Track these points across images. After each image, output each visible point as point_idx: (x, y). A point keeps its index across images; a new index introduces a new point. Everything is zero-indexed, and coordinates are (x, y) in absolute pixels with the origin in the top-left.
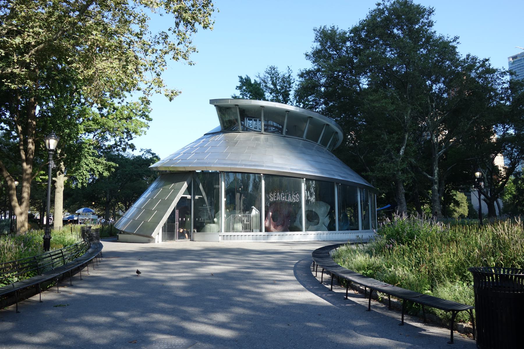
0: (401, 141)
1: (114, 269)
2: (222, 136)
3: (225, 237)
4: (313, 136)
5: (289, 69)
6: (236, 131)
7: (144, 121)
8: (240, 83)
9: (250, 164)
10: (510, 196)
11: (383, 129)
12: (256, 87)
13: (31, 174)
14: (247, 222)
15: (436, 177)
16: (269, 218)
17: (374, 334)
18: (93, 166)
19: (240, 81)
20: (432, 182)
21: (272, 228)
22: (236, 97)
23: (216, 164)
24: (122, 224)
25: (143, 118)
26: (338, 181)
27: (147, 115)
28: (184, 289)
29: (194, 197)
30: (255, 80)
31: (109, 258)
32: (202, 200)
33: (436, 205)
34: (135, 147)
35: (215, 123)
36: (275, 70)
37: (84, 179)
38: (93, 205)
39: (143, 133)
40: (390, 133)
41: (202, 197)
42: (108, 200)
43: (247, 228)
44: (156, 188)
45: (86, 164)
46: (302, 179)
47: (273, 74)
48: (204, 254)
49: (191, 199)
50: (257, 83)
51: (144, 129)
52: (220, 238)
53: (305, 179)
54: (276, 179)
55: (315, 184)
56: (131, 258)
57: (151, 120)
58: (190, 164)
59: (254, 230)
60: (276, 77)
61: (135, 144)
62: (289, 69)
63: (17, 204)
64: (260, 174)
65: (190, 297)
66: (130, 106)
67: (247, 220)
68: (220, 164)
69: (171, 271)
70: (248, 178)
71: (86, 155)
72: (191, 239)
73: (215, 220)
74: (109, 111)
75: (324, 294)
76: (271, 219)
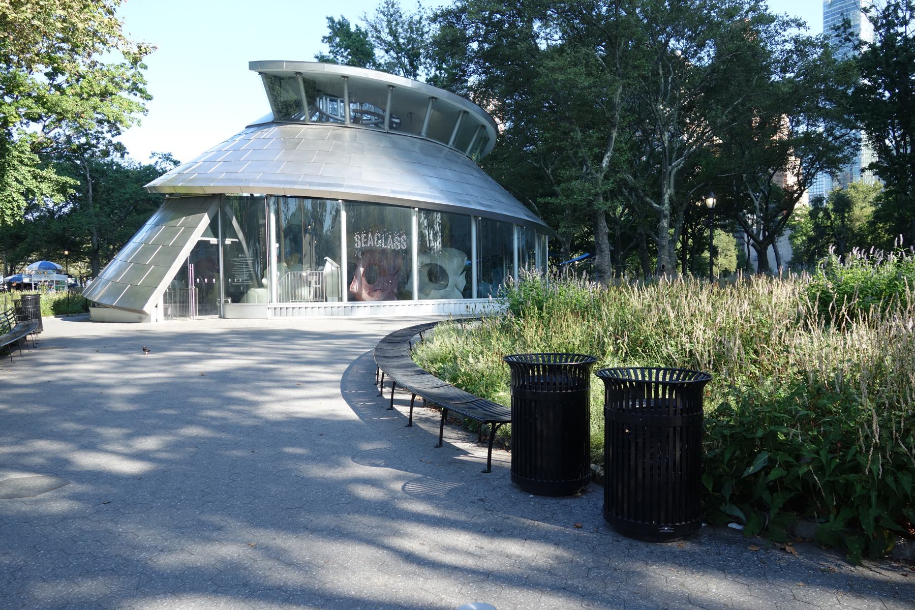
0: (604, 142)
1: (38, 368)
2: (274, 130)
3: (278, 310)
4: (439, 134)
5: (420, 5)
6: (297, 121)
7: (137, 99)
8: (331, 31)
9: (320, 181)
10: (804, 238)
11: (574, 120)
12: (358, 39)
14: (316, 284)
15: (666, 205)
16: (359, 278)
17: (377, 462)
19: (330, 27)
20: (659, 215)
21: (364, 294)
22: (323, 57)
23: (258, 181)
24: (97, 291)
25: (135, 95)
26: (476, 213)
27: (141, 89)
28: (132, 399)
29: (223, 242)
30: (357, 26)
31: (45, 348)
32: (237, 246)
33: (663, 254)
34: (125, 148)
35: (264, 109)
36: (395, 6)
37: (16, 209)
38: (67, 257)
39: (136, 122)
40: (585, 127)
41: (237, 240)
42: (96, 246)
43: (320, 296)
44: (157, 224)
45: (17, 180)
46: (412, 210)
47: (391, 15)
48: (221, 340)
49: (218, 245)
50: (361, 33)
51: (137, 115)
52: (270, 313)
53: (417, 209)
54: (363, 209)
55: (442, 219)
56: (84, 349)
57: (150, 99)
58: (212, 181)
59: (328, 298)
60: (396, 21)
61: (125, 144)
62: (420, 5)
64: (338, 200)
65: (130, 412)
66: (108, 71)
67: (316, 282)
68: (265, 181)
69: (138, 369)
70: (323, 206)
71: (16, 163)
72: (220, 314)
73: (264, 281)
74: (70, 79)
75: (361, 401)
76: (364, 279)
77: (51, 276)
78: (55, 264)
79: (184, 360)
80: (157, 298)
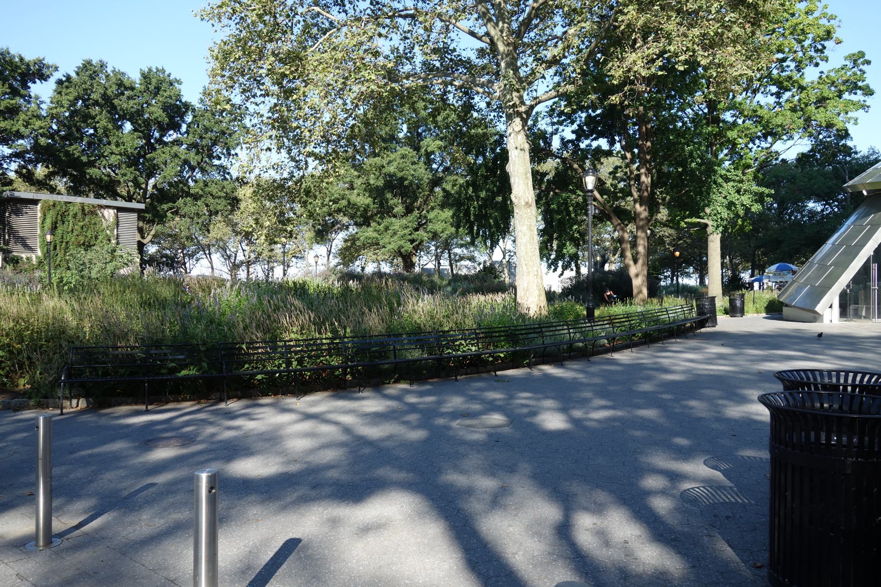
7: (858, 97)
13: (646, 218)
18: (734, 197)
25: (856, 94)
63: (631, 263)
77: (785, 277)
78: (791, 265)
79: (775, 359)
80: (832, 297)
